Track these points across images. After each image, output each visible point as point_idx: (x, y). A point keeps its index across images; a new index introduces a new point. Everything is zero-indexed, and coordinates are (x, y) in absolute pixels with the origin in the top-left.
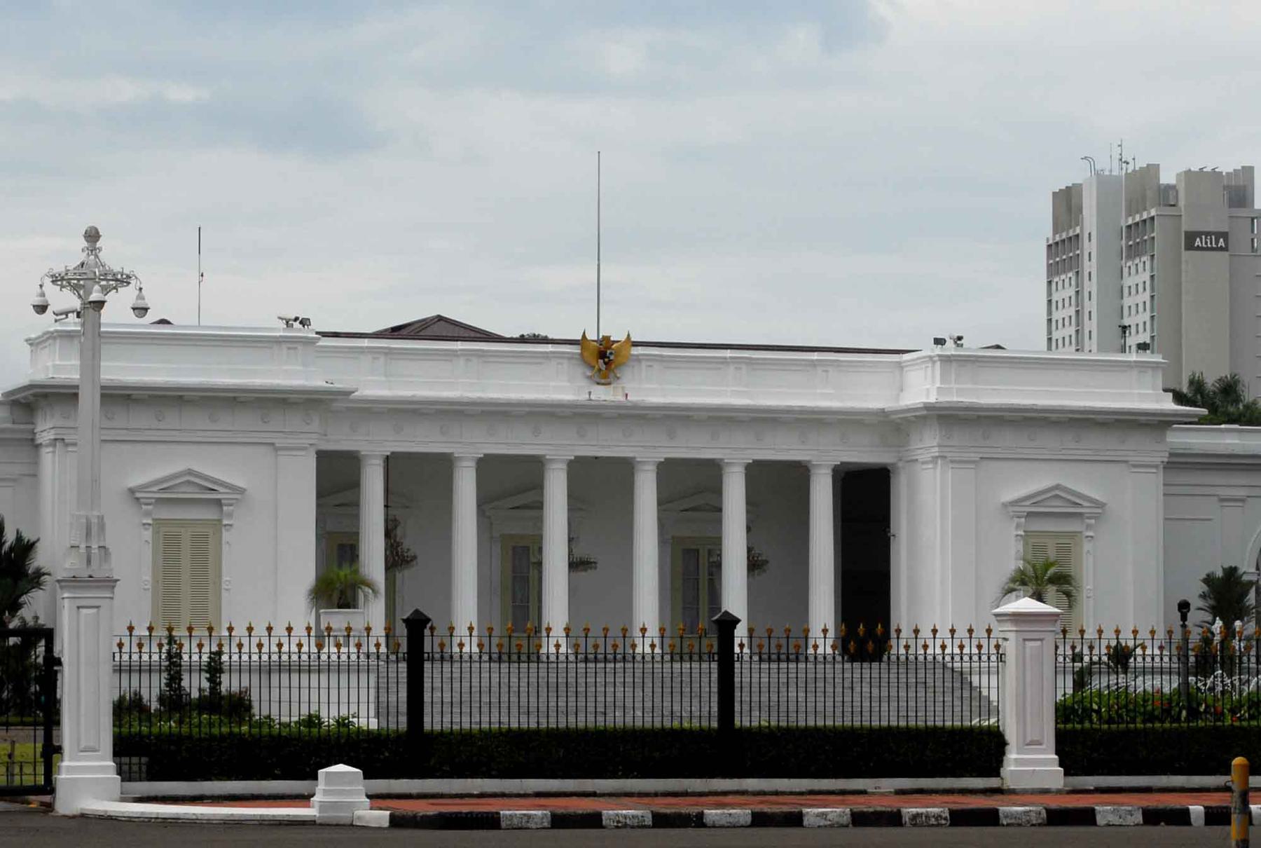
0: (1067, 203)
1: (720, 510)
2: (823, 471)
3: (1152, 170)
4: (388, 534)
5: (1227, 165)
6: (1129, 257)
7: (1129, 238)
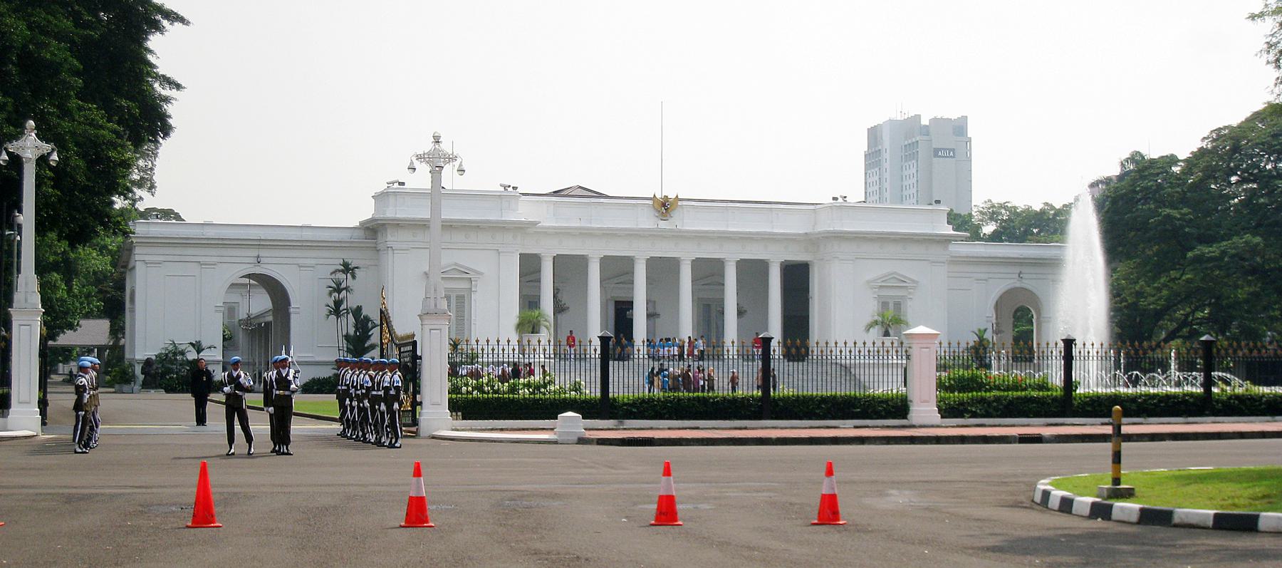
0: (874, 134)
1: (632, 283)
3: (918, 117)
5: (954, 116)
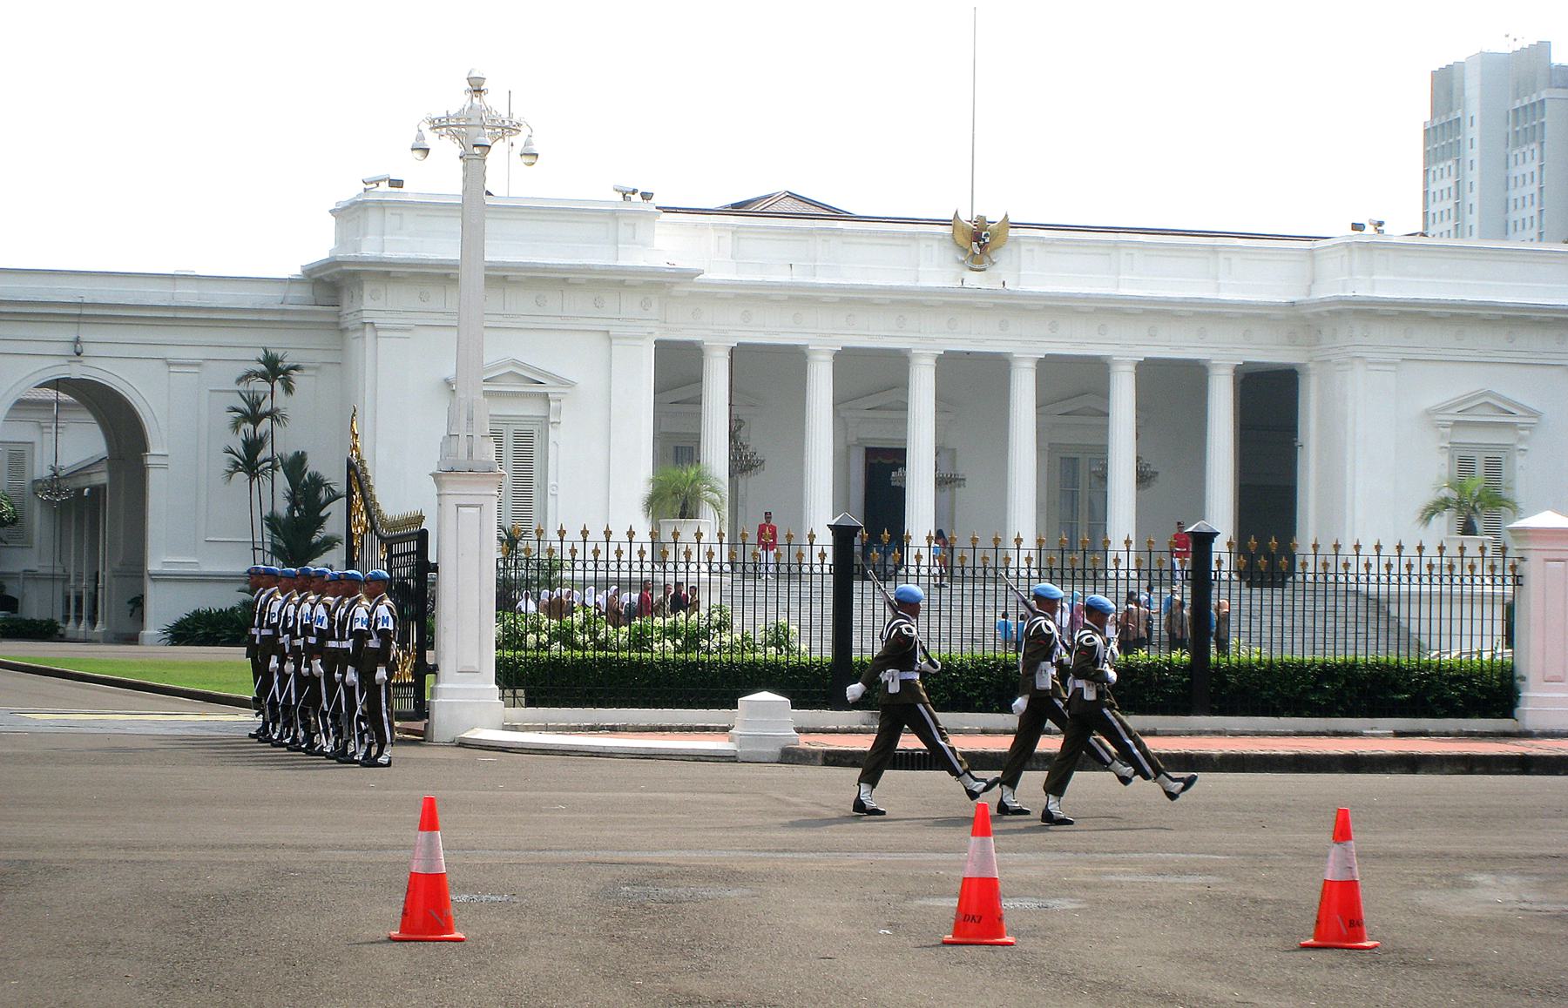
0: (1445, 85)
2: (1223, 371)
4: (732, 436)
6: (1517, 145)
7: (1516, 123)
